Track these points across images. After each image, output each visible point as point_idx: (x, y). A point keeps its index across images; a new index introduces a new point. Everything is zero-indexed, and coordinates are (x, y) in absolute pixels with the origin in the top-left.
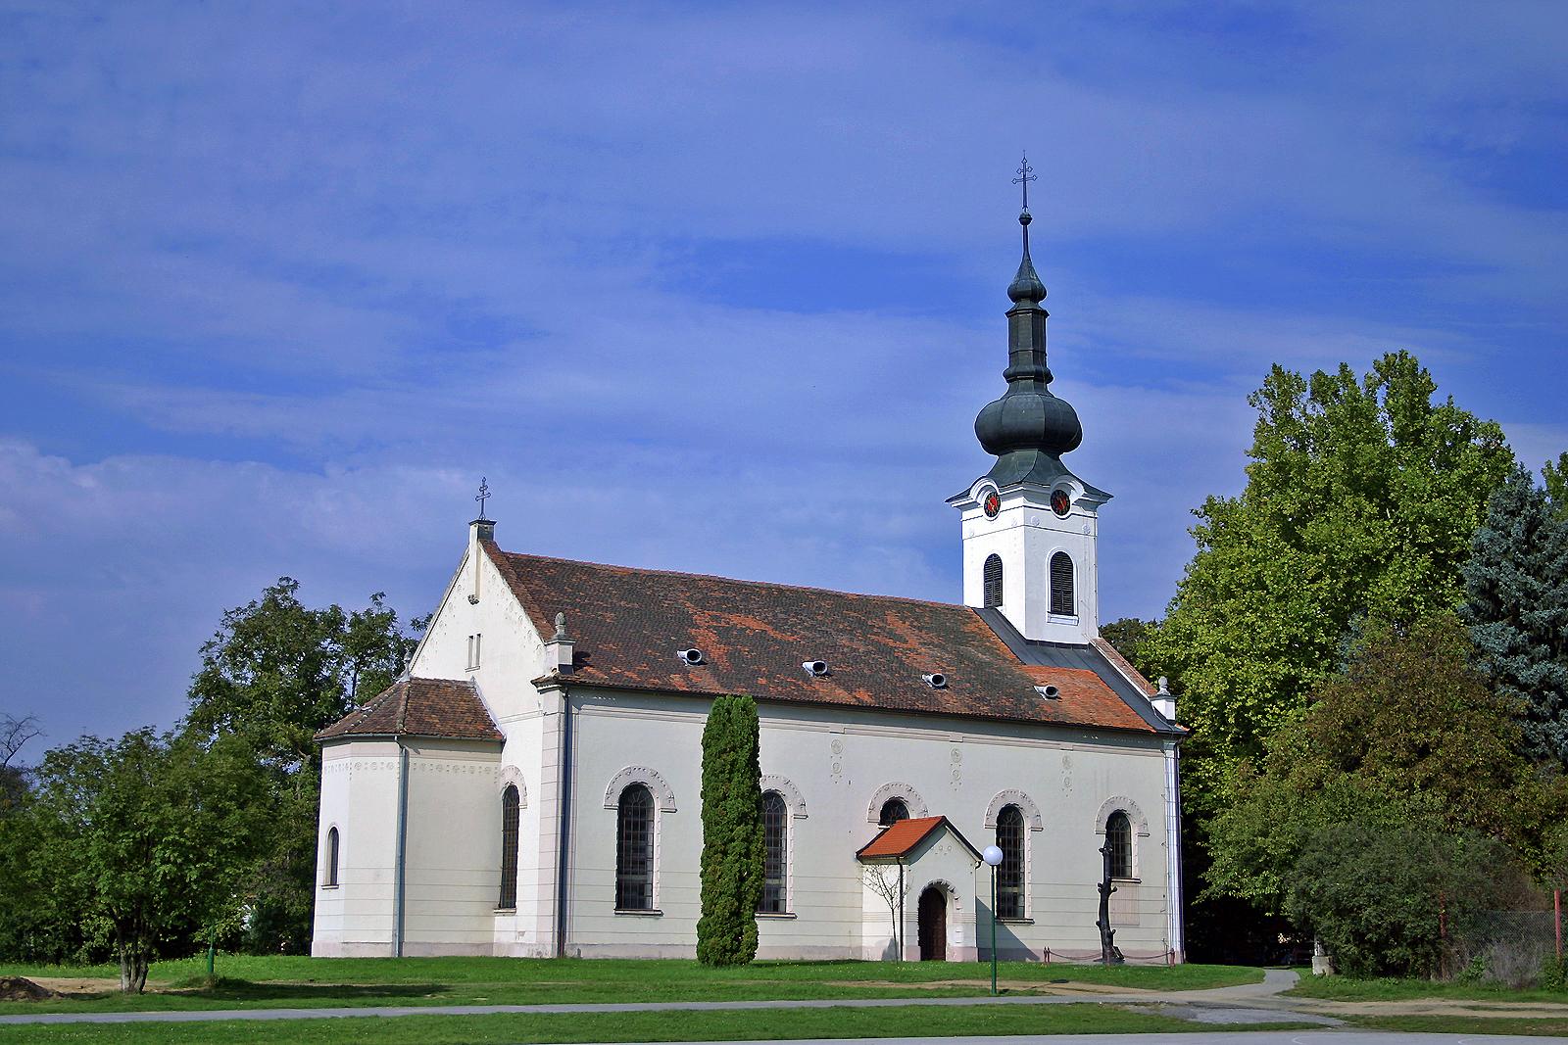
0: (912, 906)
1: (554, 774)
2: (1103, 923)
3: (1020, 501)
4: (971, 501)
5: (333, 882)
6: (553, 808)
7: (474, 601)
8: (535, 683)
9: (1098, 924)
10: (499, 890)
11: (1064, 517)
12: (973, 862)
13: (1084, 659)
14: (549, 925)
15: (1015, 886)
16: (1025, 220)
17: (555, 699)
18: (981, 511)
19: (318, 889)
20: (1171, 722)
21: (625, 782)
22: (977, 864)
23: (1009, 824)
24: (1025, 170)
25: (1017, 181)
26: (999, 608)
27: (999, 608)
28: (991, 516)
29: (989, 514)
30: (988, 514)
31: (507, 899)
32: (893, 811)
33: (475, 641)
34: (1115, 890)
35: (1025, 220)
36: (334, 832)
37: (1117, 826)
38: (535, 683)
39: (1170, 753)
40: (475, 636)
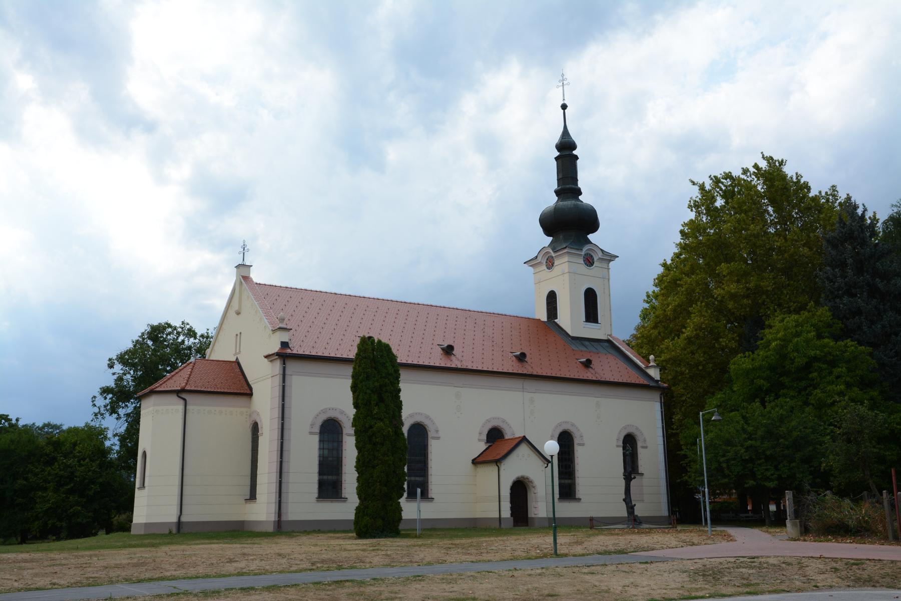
0: (506, 492)
1: (277, 413)
2: (628, 499)
3: (566, 259)
4: (538, 262)
5: (143, 486)
6: (276, 434)
7: (238, 313)
8: (266, 357)
9: (624, 500)
10: (258, 483)
11: (591, 268)
12: (543, 464)
13: (606, 344)
14: (273, 508)
15: (570, 479)
16: (564, 107)
17: (278, 364)
18: (544, 267)
19: (136, 490)
20: (657, 381)
21: (324, 417)
22: (546, 465)
23: (566, 440)
24: (563, 80)
25: (560, 86)
26: (556, 320)
27: (556, 320)
28: (549, 269)
29: (548, 268)
30: (548, 268)
31: (253, 496)
32: (495, 435)
33: (238, 337)
34: (635, 478)
35: (564, 107)
36: (144, 454)
37: (630, 443)
38: (266, 357)
39: (104, 530)
40: (239, 335)
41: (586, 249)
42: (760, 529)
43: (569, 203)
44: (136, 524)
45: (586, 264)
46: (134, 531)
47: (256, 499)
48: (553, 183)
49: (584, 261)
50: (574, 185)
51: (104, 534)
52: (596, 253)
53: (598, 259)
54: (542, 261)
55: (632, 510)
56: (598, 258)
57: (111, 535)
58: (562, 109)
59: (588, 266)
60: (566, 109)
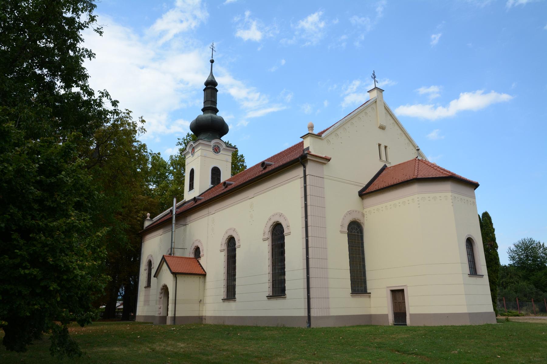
16: (212, 62)
35: (212, 62)
41: (213, 143)
42: (364, 227)
43: (209, 115)
44: (250, 168)
45: (214, 152)
46: (137, 320)
47: (150, 286)
48: (200, 104)
49: (213, 150)
50: (215, 106)
51: (185, 230)
52: (221, 145)
53: (223, 149)
54: (189, 151)
55: (283, 271)
56: (223, 148)
57: (193, 197)
58: (211, 62)
59: (215, 153)
60: (213, 63)
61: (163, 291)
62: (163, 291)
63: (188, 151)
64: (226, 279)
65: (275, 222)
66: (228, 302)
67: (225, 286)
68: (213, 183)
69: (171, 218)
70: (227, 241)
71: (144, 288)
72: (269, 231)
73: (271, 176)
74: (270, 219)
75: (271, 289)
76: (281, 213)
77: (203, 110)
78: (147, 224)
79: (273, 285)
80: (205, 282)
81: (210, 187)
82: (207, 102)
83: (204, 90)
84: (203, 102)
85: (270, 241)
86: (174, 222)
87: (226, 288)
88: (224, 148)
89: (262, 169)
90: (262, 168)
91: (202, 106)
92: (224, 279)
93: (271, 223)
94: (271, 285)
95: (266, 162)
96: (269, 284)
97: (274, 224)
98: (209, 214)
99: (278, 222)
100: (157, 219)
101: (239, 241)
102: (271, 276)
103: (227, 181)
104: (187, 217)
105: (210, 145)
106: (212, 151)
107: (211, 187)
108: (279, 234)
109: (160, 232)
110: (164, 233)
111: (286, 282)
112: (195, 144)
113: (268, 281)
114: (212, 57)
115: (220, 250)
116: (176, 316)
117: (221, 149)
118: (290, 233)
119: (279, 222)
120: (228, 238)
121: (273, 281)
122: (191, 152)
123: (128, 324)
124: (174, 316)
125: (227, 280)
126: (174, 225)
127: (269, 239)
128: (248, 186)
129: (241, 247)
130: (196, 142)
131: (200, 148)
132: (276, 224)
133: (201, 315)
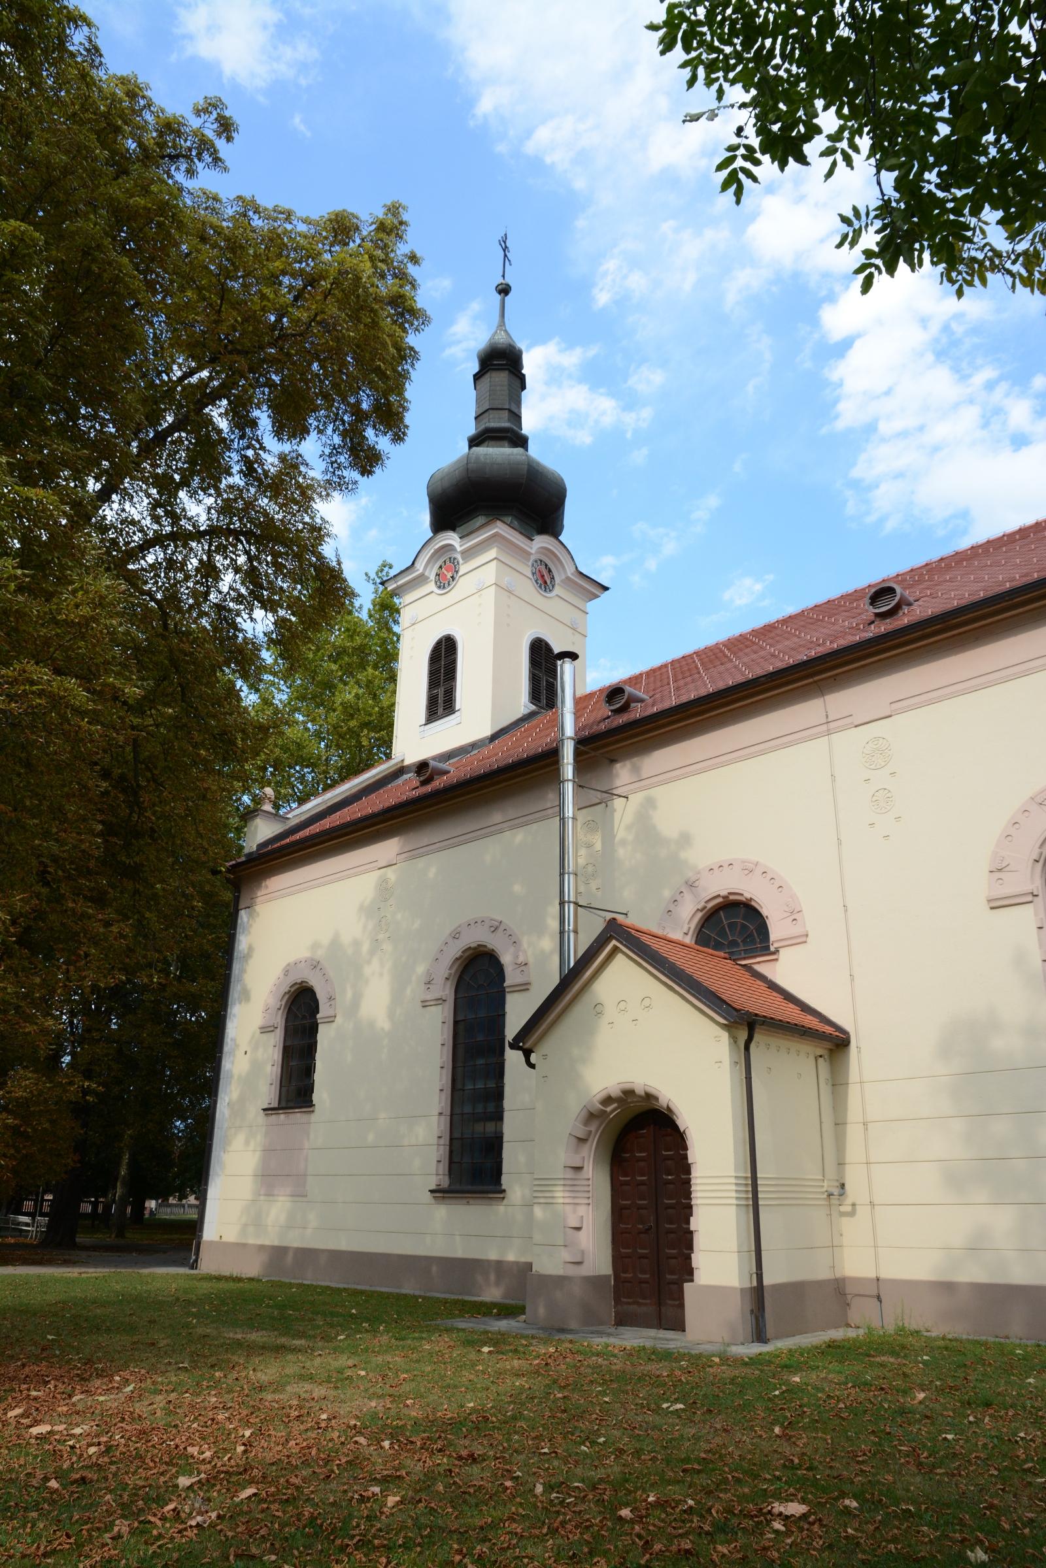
16: (504, 290)
45: (536, 581)
52: (559, 565)
54: (426, 574)
55: (491, 1108)
58: (500, 292)
59: (540, 587)
61: (593, 1128)
62: (593, 1128)
63: (422, 575)
64: (449, 1113)
65: (296, 984)
66: (465, 1201)
67: (442, 1141)
68: (535, 696)
69: (551, 756)
70: (287, 1001)
71: (261, 1118)
72: (446, 976)
73: (631, 744)
74: (456, 935)
75: (444, 1167)
76: (499, 918)
77: (474, 442)
78: (262, 831)
79: (451, 1152)
80: (838, 1084)
81: (527, 711)
82: (495, 411)
83: (477, 377)
84: (474, 415)
85: (449, 1006)
86: (568, 771)
87: (448, 1147)
88: (568, 578)
89: (418, 784)
90: (606, 710)
91: (471, 430)
92: (441, 1114)
93: (455, 950)
94: (444, 1152)
95: (432, 763)
96: (438, 1150)
97: (293, 990)
98: (829, 727)
99: (482, 949)
100: (303, 818)
101: (332, 1002)
102: (445, 1121)
103: (434, 758)
104: (613, 761)
105: (529, 554)
106: (531, 576)
107: (529, 711)
108: (304, 1017)
109: (388, 849)
110: (413, 854)
111: (505, 1145)
112: (465, 540)
113: (435, 1141)
114: (503, 276)
115: (989, 901)
116: (767, 1281)
117: (557, 580)
118: (807, 935)
119: (485, 946)
120: (461, 957)
121: (451, 1139)
122: (432, 577)
123: (485, 1344)
124: (755, 1284)
125: (452, 1115)
126: (569, 788)
127: (278, 1031)
128: (469, 796)
129: (809, 940)
130: (489, 528)
131: (492, 553)
132: (298, 989)
133: (838, 1275)
